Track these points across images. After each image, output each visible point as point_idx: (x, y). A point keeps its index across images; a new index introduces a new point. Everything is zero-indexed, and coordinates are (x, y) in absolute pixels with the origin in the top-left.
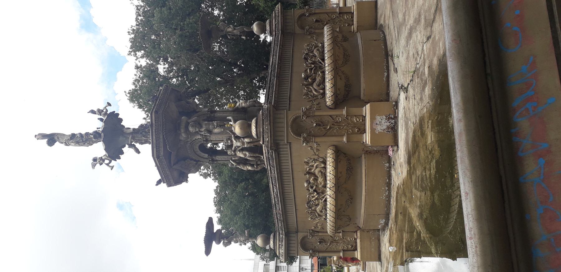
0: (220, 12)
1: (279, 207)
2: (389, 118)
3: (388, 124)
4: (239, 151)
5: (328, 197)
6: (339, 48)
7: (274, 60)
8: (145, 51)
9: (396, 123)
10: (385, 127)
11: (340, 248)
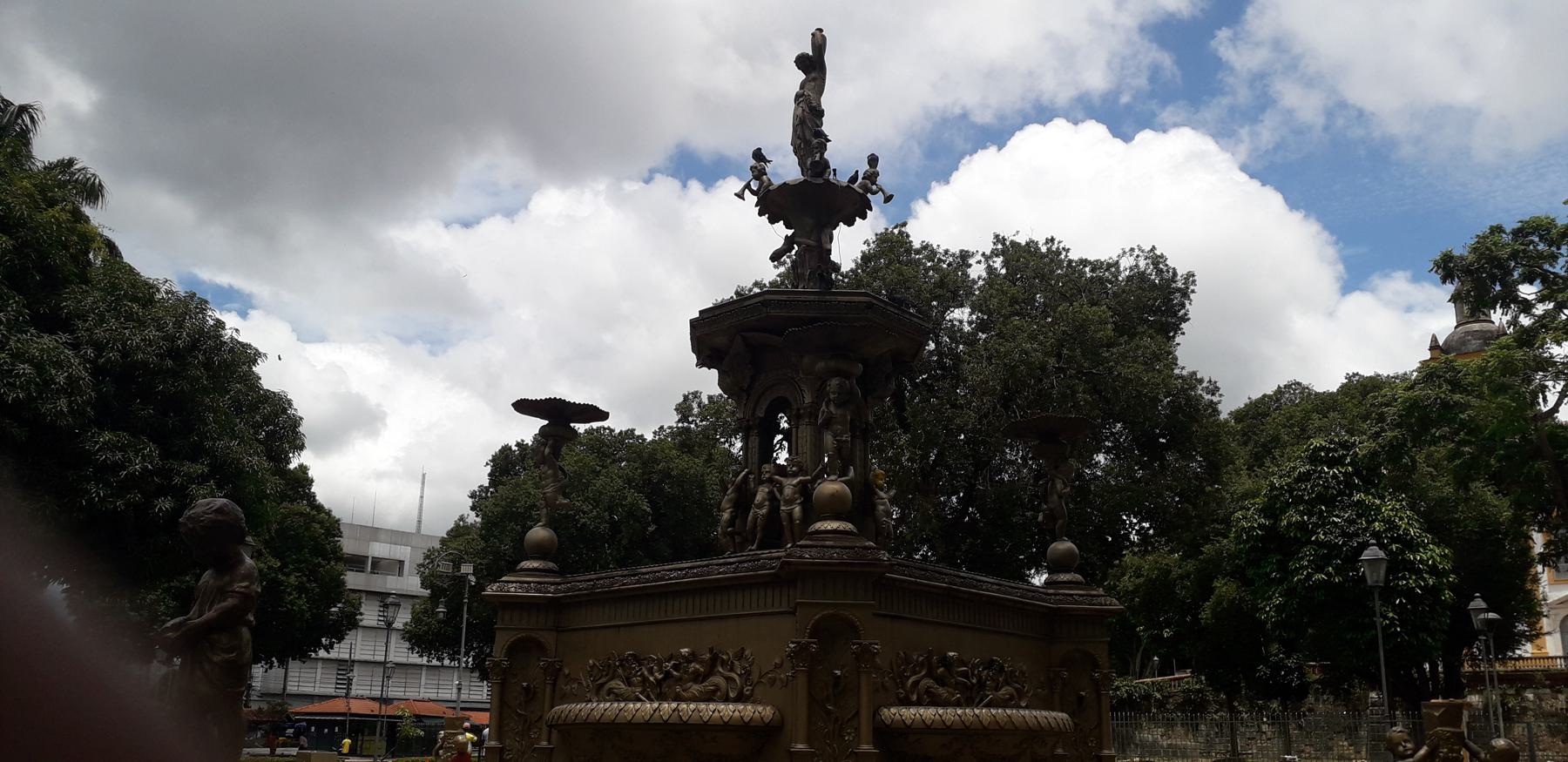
0: (1103, 470)
1: (631, 583)
4: (771, 493)
5: (656, 705)
7: (989, 585)
8: (1005, 277)
11: (508, 742)
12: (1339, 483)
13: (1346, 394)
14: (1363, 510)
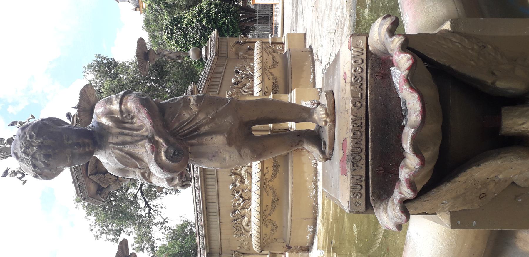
12: (179, 31)
13: (149, 29)
14: (189, 24)
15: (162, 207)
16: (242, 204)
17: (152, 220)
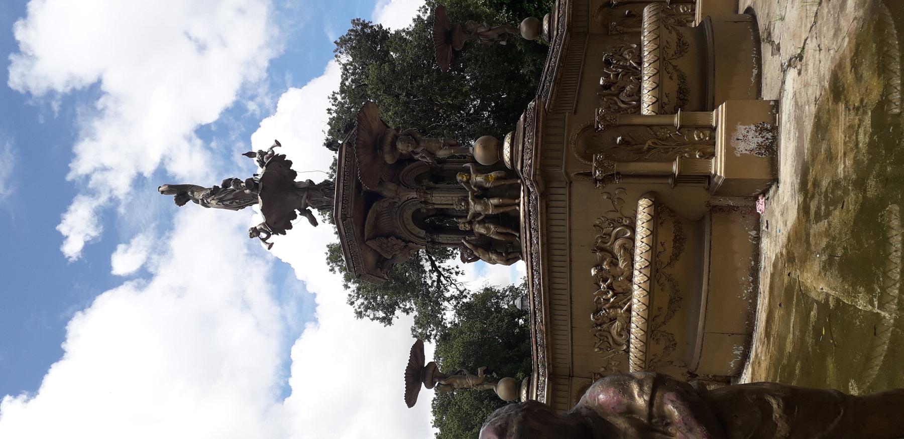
2: (761, 130)
3: (760, 140)
4: (479, 222)
6: (670, 32)
9: (775, 140)
10: (753, 146)
15: (457, 273)
16: (612, 300)
17: (442, 292)
